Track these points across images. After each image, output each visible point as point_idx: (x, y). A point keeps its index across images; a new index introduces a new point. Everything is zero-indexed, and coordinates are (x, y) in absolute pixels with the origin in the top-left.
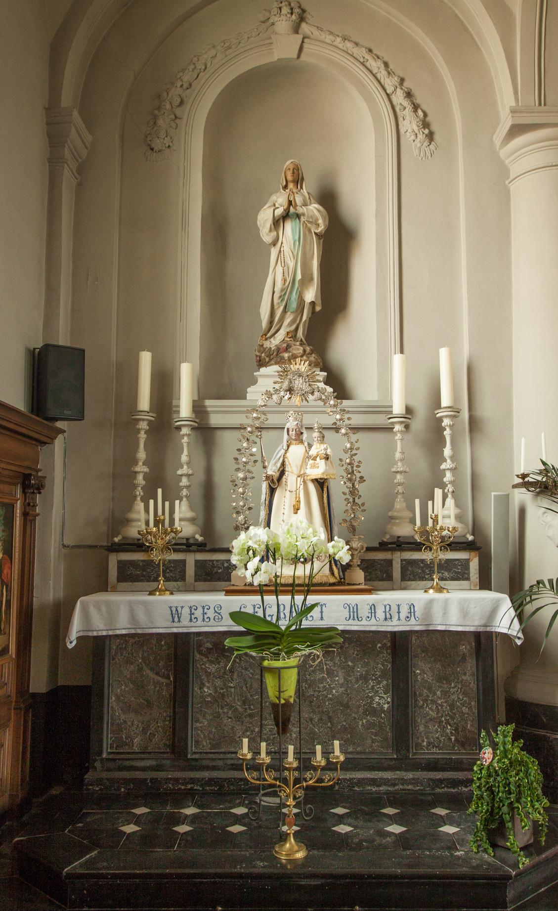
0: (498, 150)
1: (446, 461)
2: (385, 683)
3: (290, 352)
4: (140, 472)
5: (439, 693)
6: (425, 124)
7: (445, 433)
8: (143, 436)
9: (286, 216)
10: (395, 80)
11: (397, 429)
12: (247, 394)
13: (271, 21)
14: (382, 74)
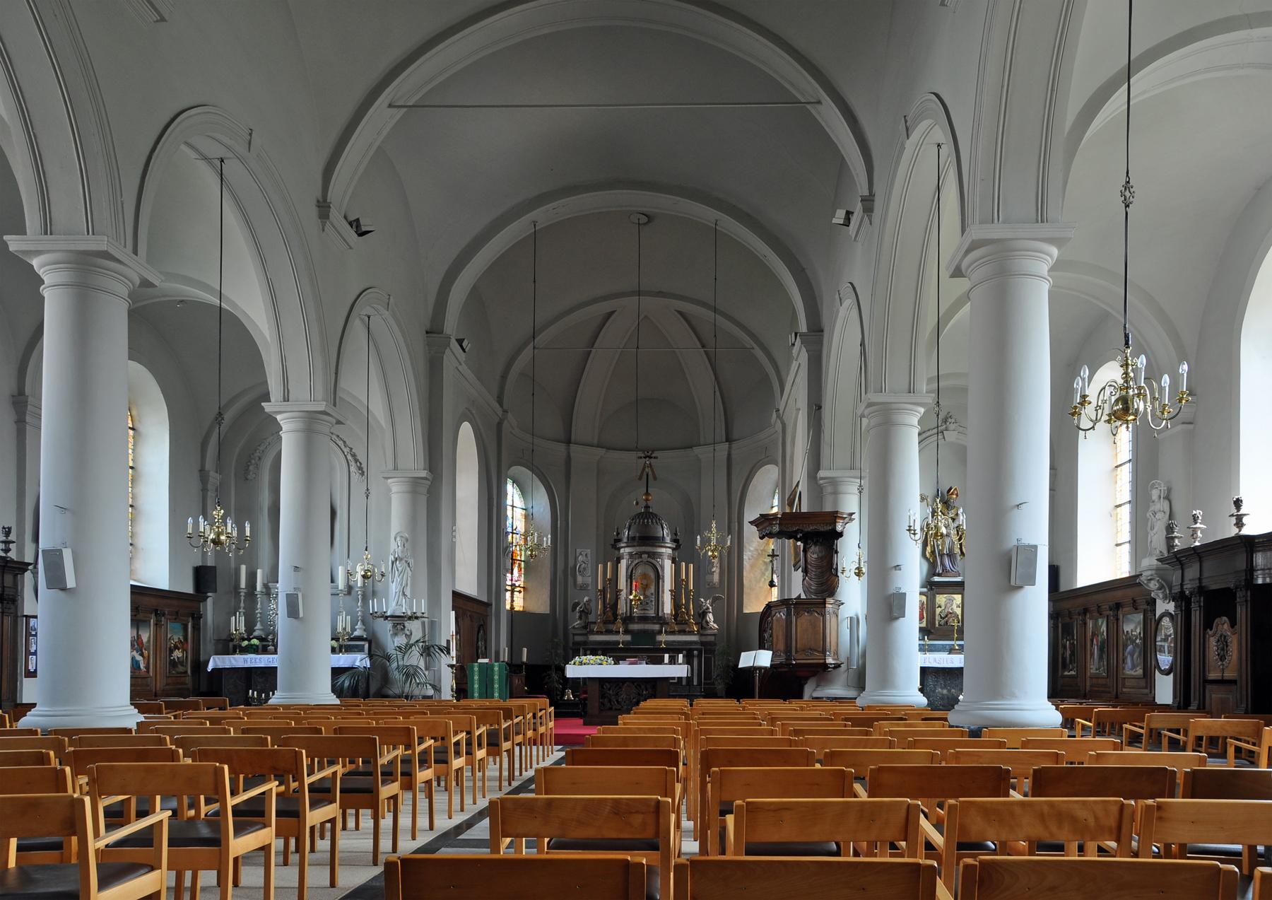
8: (242, 598)
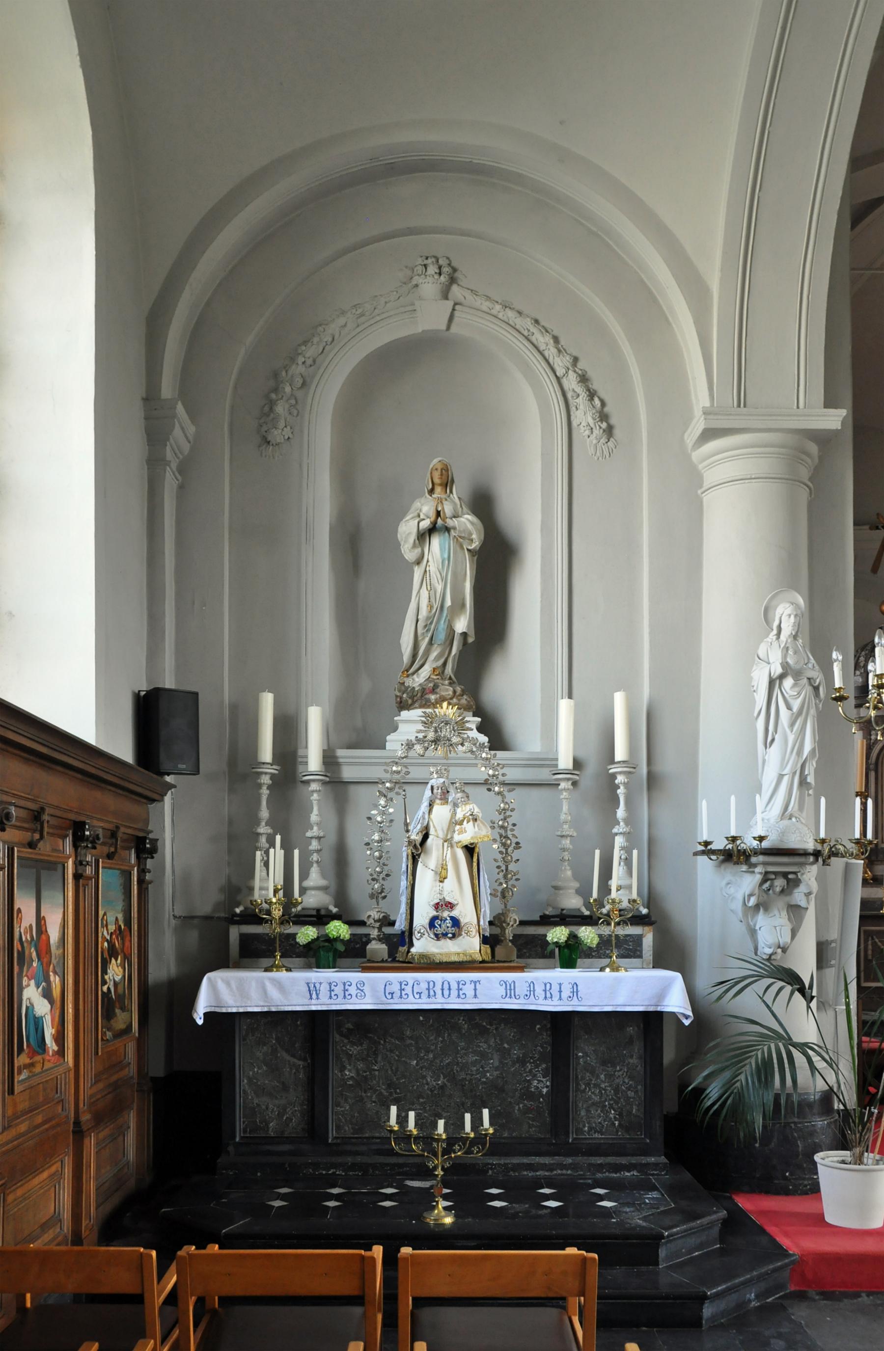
0: (689, 451)
1: (618, 824)
2: (544, 1066)
3: (437, 693)
4: (263, 833)
5: (602, 1076)
6: (603, 416)
7: (619, 791)
8: (265, 792)
9: (432, 530)
10: (567, 360)
11: (563, 787)
12: (387, 743)
13: (414, 282)
14: (551, 352)
